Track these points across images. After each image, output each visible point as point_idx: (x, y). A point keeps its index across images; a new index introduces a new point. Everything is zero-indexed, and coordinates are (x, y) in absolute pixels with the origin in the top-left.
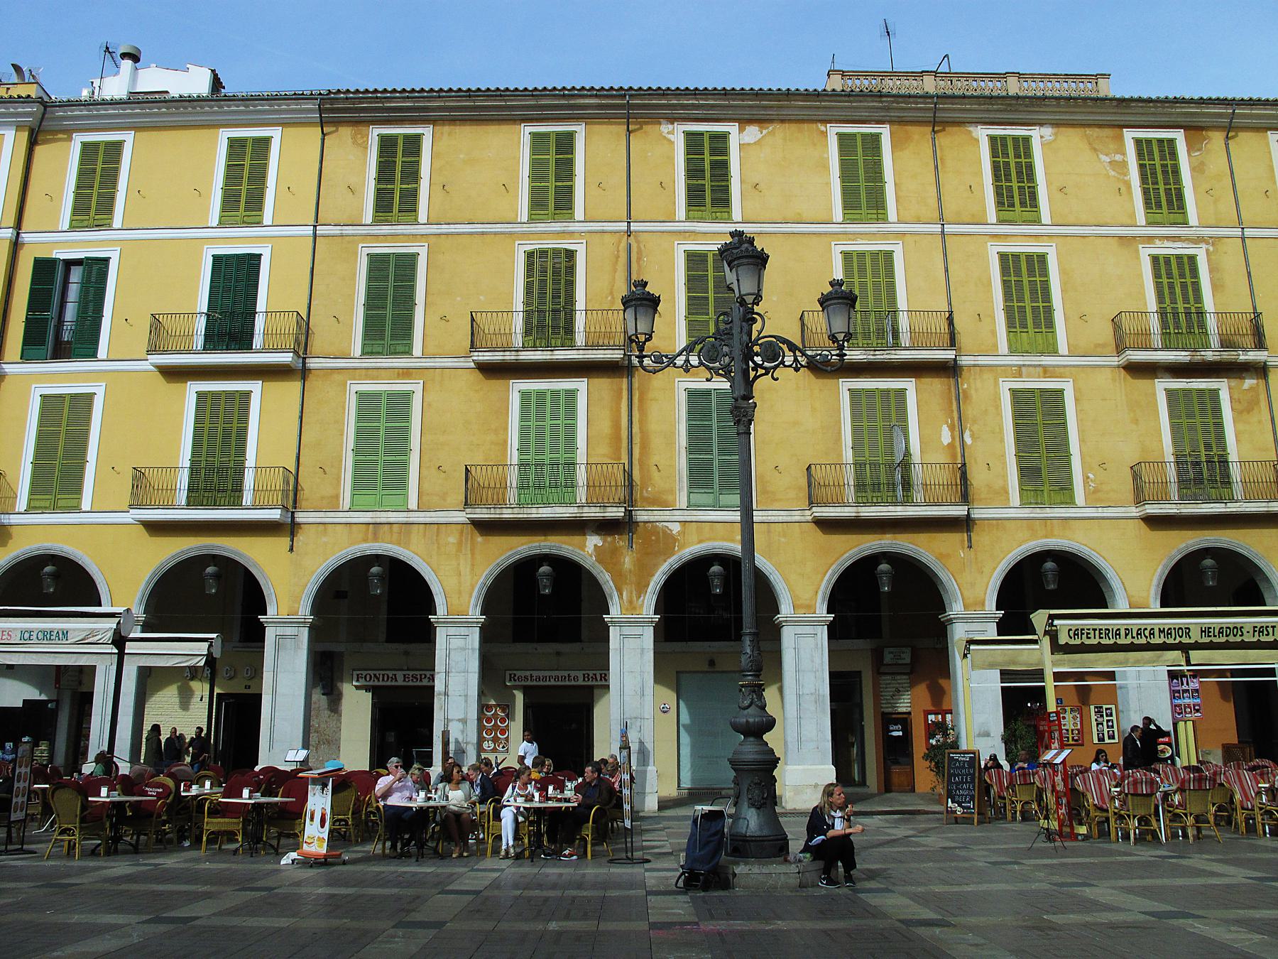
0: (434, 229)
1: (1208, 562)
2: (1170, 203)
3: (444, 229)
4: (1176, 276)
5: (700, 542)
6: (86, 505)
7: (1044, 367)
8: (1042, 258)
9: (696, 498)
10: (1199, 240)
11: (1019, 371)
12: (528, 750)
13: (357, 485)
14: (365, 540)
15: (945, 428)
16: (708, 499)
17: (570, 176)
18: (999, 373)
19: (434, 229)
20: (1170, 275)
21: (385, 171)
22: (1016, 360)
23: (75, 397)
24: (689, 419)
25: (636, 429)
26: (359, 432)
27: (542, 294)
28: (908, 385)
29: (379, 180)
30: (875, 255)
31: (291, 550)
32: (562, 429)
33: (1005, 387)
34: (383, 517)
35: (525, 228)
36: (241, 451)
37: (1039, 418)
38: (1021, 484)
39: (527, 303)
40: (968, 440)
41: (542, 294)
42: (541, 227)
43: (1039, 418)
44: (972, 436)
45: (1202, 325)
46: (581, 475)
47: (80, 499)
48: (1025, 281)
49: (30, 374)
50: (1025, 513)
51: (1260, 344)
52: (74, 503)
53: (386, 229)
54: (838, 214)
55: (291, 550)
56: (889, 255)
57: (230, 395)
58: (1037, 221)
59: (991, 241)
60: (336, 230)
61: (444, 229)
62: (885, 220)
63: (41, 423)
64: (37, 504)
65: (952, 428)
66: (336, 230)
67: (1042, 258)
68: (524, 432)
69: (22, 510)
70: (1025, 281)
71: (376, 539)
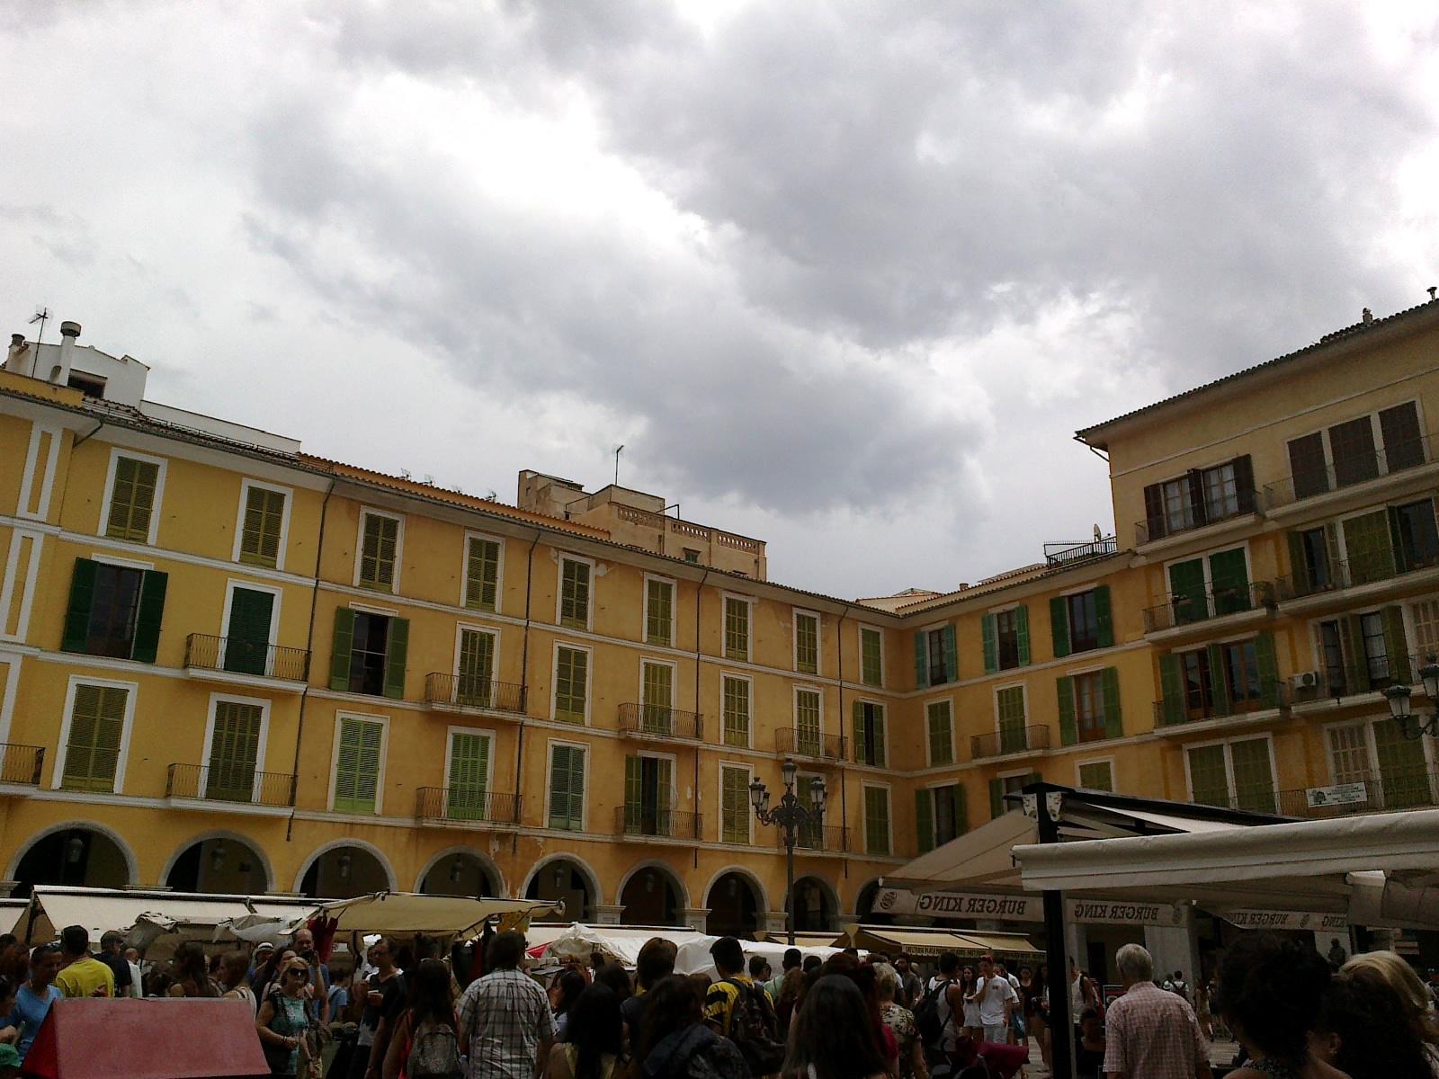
0: (404, 601)
1: (734, 881)
2: (809, 658)
3: (412, 602)
4: (658, 677)
5: (554, 852)
6: (118, 788)
7: (741, 755)
8: (746, 683)
9: (555, 821)
10: (819, 685)
11: (728, 756)
12: (51, 988)
13: (340, 792)
14: (344, 836)
15: (689, 789)
16: (563, 823)
17: (494, 578)
18: (547, 728)
19: (404, 601)
20: (473, 649)
21: (369, 547)
22: (728, 750)
23: (110, 691)
24: (554, 766)
25: (522, 770)
26: (343, 751)
27: (472, 666)
28: (491, 734)
29: (366, 551)
30: (662, 667)
31: (288, 839)
32: (479, 764)
33: (722, 764)
34: (358, 819)
35: (465, 612)
36: (253, 757)
37: (567, 762)
38: (724, 828)
39: (462, 669)
40: (700, 798)
41: (472, 666)
42: (474, 613)
43: (567, 762)
44: (702, 796)
45: (818, 739)
46: (488, 800)
47: (113, 783)
48: (572, 667)
49: (69, 665)
50: (725, 847)
51: (698, 736)
52: (109, 785)
53: (370, 594)
54: (357, 581)
55: (288, 839)
56: (491, 637)
57: (246, 708)
58: (274, 567)
59: (556, 637)
60: (334, 587)
61: (412, 602)
62: (144, 541)
63: (77, 709)
64: (70, 783)
65: (692, 790)
66: (334, 587)
67: (746, 683)
68: (454, 763)
69: (57, 788)
70: (572, 667)
71: (351, 835)
